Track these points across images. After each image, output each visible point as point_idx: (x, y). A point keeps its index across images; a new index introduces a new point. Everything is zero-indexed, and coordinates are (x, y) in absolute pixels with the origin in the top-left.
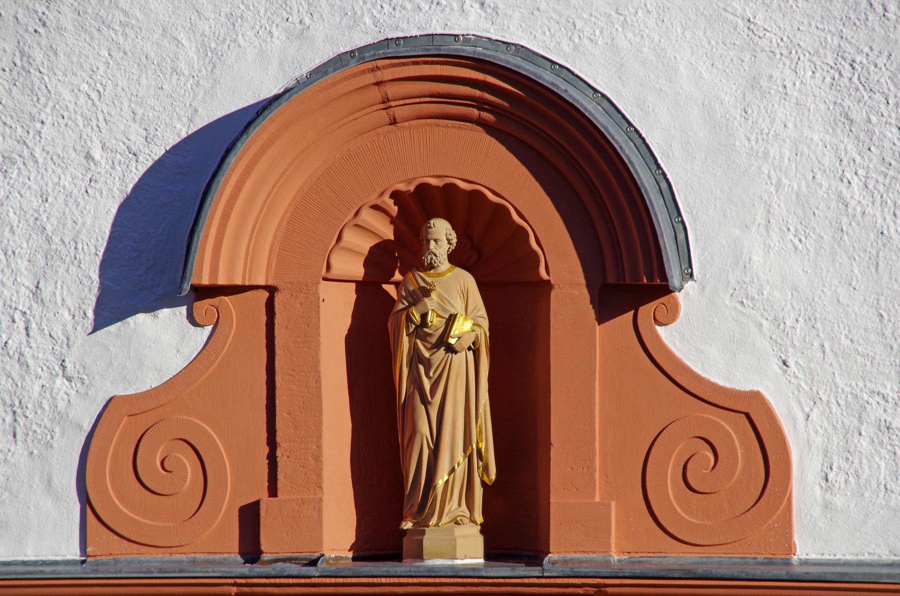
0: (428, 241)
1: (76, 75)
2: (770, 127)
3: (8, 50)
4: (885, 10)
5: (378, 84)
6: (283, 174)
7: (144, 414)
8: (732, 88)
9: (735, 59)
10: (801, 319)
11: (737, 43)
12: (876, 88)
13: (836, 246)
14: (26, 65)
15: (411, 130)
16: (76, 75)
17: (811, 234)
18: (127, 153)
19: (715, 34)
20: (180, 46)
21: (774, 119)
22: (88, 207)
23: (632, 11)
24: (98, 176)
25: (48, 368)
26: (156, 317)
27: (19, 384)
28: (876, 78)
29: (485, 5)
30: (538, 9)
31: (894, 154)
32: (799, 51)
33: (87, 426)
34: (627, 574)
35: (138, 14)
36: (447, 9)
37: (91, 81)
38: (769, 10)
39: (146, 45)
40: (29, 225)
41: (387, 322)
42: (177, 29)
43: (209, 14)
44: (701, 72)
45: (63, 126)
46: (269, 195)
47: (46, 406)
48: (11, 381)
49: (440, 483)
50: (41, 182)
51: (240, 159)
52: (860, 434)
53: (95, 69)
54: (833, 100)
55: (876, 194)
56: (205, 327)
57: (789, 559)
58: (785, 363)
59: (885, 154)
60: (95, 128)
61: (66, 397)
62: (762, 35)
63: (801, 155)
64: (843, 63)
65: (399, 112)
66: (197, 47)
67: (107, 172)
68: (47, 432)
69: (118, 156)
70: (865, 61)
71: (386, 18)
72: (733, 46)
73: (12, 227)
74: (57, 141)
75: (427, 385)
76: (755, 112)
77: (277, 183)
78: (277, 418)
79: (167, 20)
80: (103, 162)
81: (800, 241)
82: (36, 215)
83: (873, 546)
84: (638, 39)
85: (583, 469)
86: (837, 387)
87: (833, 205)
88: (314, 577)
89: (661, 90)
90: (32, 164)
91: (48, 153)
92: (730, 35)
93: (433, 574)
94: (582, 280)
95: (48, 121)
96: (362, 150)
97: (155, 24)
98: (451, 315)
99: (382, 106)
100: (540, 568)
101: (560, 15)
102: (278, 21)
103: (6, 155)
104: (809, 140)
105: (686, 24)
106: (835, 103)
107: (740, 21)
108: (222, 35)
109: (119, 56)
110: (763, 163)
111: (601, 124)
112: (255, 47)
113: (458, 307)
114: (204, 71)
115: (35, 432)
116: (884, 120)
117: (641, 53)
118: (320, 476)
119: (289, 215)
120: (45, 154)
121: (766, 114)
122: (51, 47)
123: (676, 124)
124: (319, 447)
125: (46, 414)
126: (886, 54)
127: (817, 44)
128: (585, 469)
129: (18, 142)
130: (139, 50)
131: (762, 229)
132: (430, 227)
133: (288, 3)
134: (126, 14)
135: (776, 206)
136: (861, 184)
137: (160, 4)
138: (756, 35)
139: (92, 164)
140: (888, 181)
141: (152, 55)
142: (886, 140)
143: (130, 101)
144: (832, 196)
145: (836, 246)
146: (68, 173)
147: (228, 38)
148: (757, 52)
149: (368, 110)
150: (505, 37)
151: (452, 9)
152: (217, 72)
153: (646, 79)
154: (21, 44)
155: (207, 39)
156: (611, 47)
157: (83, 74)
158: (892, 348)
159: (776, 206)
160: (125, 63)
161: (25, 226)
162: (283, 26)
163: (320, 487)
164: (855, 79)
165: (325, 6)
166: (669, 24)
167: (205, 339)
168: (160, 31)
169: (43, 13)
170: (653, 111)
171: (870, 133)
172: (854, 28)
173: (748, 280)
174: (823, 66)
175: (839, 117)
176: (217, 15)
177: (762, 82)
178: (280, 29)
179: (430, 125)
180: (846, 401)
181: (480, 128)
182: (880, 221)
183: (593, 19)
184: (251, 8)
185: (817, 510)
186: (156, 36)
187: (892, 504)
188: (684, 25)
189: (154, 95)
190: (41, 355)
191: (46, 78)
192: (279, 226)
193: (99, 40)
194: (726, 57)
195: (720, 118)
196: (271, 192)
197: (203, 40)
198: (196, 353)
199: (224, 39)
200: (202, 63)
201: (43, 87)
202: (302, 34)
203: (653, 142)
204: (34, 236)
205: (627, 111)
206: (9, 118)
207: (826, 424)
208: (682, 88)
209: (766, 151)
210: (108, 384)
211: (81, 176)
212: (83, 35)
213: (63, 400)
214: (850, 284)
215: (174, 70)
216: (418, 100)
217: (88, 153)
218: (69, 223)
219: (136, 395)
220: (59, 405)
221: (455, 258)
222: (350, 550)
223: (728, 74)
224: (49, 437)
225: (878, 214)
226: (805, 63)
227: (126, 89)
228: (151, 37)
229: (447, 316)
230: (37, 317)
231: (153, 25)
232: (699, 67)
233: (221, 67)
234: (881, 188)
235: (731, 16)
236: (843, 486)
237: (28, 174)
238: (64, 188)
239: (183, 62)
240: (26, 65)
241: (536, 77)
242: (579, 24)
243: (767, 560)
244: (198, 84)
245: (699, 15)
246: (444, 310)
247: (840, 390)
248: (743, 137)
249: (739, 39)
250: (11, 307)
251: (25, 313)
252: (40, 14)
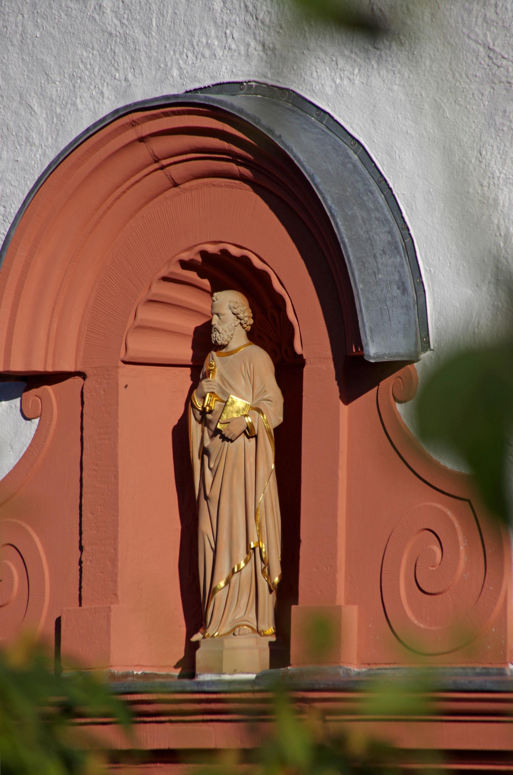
2: (501, 169)
8: (471, 127)
11: (478, 74)
15: (193, 192)
19: (460, 65)
20: (33, 113)
38: (508, 35)
39: (7, 115)
42: (30, 95)
43: (55, 76)
44: (444, 109)
56: (33, 420)
57: (503, 669)
66: (47, 114)
71: (189, 69)
72: (475, 78)
76: (489, 154)
85: (326, 568)
89: (407, 133)
92: (473, 66)
94: (329, 354)
96: (153, 217)
97: (13, 91)
105: (434, 55)
107: (481, 49)
110: (493, 211)
111: (307, 172)
114: (50, 139)
117: (392, 92)
121: (498, 155)
123: (420, 171)
124: (116, 549)
128: (329, 568)
133: (116, 59)
137: (17, 69)
138: (495, 64)
148: (495, 83)
150: (279, 82)
153: (395, 121)
155: (54, 104)
156: (366, 86)
162: (112, 84)
163: (116, 595)
165: (145, 59)
168: (18, 99)
170: (399, 157)
176: (62, 77)
178: (110, 87)
181: (248, 187)
184: (88, 66)
186: (15, 104)
188: (433, 56)
189: (12, 169)
194: (468, 91)
195: (458, 162)
203: (399, 192)
205: (377, 159)
208: (425, 129)
209: (496, 198)
216: (184, 157)
222: (176, 667)
223: (469, 111)
228: (11, 105)
231: (12, 92)
232: (443, 104)
233: (62, 134)
235: (474, 43)
239: (35, 131)
241: (255, 123)
243: (484, 671)
245: (446, 44)
248: (477, 182)
249: (480, 69)
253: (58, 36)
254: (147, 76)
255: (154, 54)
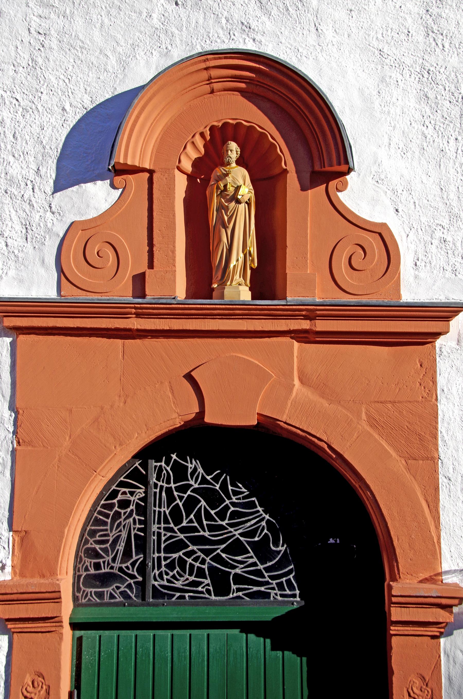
0: (227, 151)
1: (58, 71)
3: (26, 58)
4: (443, 47)
5: (207, 69)
6: (159, 114)
7: (89, 230)
9: (374, 68)
10: (404, 190)
11: (375, 61)
12: (439, 83)
13: (421, 156)
14: (34, 65)
16: (58, 71)
17: (409, 150)
18: (82, 108)
21: (392, 96)
22: (63, 133)
23: (326, 44)
24: (68, 118)
25: (43, 207)
26: (95, 184)
27: (29, 215)
28: (440, 78)
29: (256, 40)
30: (281, 43)
31: (448, 114)
32: (404, 65)
33: (61, 235)
34: (328, 304)
35: (88, 42)
36: (237, 42)
37: (65, 74)
40: (35, 140)
41: (206, 190)
45: (51, 95)
46: (152, 124)
47: (42, 225)
48: (25, 213)
49: (232, 266)
50: (41, 121)
51: (141, 100)
52: (432, 244)
53: (67, 68)
54: (420, 88)
55: (440, 133)
58: (397, 210)
59: (443, 114)
60: (67, 96)
61: (51, 221)
62: (386, 57)
63: (405, 113)
64: (424, 71)
65: (216, 86)
67: (72, 117)
68: (42, 237)
69: (78, 110)
70: (434, 70)
73: (26, 141)
74: (49, 102)
75: (226, 218)
77: (156, 118)
78: (154, 232)
79: (102, 46)
80: (71, 112)
81: (404, 154)
82: (38, 136)
83: (438, 295)
84: (328, 57)
86: (421, 222)
87: (420, 137)
88: (174, 304)
90: (36, 112)
91: (44, 107)
93: (233, 303)
95: (45, 93)
98: (238, 186)
99: (208, 82)
100: (285, 301)
101: (292, 46)
102: (155, 47)
103: (24, 107)
104: (408, 107)
106: (420, 90)
107: (376, 50)
108: (128, 54)
109: (79, 62)
112: (144, 60)
113: (241, 182)
115: (37, 237)
116: (443, 98)
118: (174, 260)
119: (161, 136)
120: (43, 108)
122: (46, 57)
124: (174, 247)
125: (42, 229)
126: (444, 67)
127: (412, 62)
129: (30, 102)
130: (89, 60)
131: (387, 148)
132: (229, 144)
134: (83, 42)
135: (393, 137)
136: (433, 128)
139: (65, 113)
140: (445, 126)
141: (95, 62)
142: (444, 107)
143: (84, 84)
144: (419, 133)
145: (421, 156)
146: (54, 117)
147: (131, 55)
149: (201, 84)
151: (240, 42)
152: (126, 71)
154: (32, 55)
157: (62, 71)
158: (446, 204)
159: (393, 137)
160: (82, 66)
161: (33, 141)
163: (175, 266)
164: (430, 79)
166: (343, 51)
167: (119, 195)
168: (99, 51)
169: (43, 41)
171: (437, 104)
172: (429, 55)
173: (380, 171)
174: (415, 72)
175: (422, 96)
176: (126, 44)
177: (386, 79)
178: (156, 51)
179: (230, 94)
180: (425, 228)
182: (441, 145)
183: (307, 47)
184: (143, 41)
185: (412, 279)
187: (447, 276)
190: (40, 201)
191: (44, 71)
192: (156, 141)
193: (69, 54)
196: (153, 122)
197: (119, 56)
198: (115, 201)
199: (130, 56)
200: (118, 67)
201: (42, 76)
202: (167, 53)
204: (37, 145)
206: (26, 90)
207: (416, 239)
210: (72, 215)
211: (60, 119)
212: (62, 52)
213: (50, 222)
214: (427, 174)
215: (105, 70)
216: (225, 80)
217: (63, 108)
218: (54, 139)
219: (85, 221)
220: (48, 225)
221: (238, 163)
224: (43, 240)
225: (441, 141)
226: (406, 71)
227: (82, 78)
229: (236, 186)
230: (38, 183)
234: (442, 129)
236: (424, 267)
237: (34, 117)
238: (52, 124)
240: (34, 65)
242: (301, 50)
244: (117, 76)
246: (235, 183)
247: (422, 223)
250: (25, 178)
251: (32, 181)
252: (41, 41)
253: (124, 26)
254: (180, 48)
255: (184, 39)
